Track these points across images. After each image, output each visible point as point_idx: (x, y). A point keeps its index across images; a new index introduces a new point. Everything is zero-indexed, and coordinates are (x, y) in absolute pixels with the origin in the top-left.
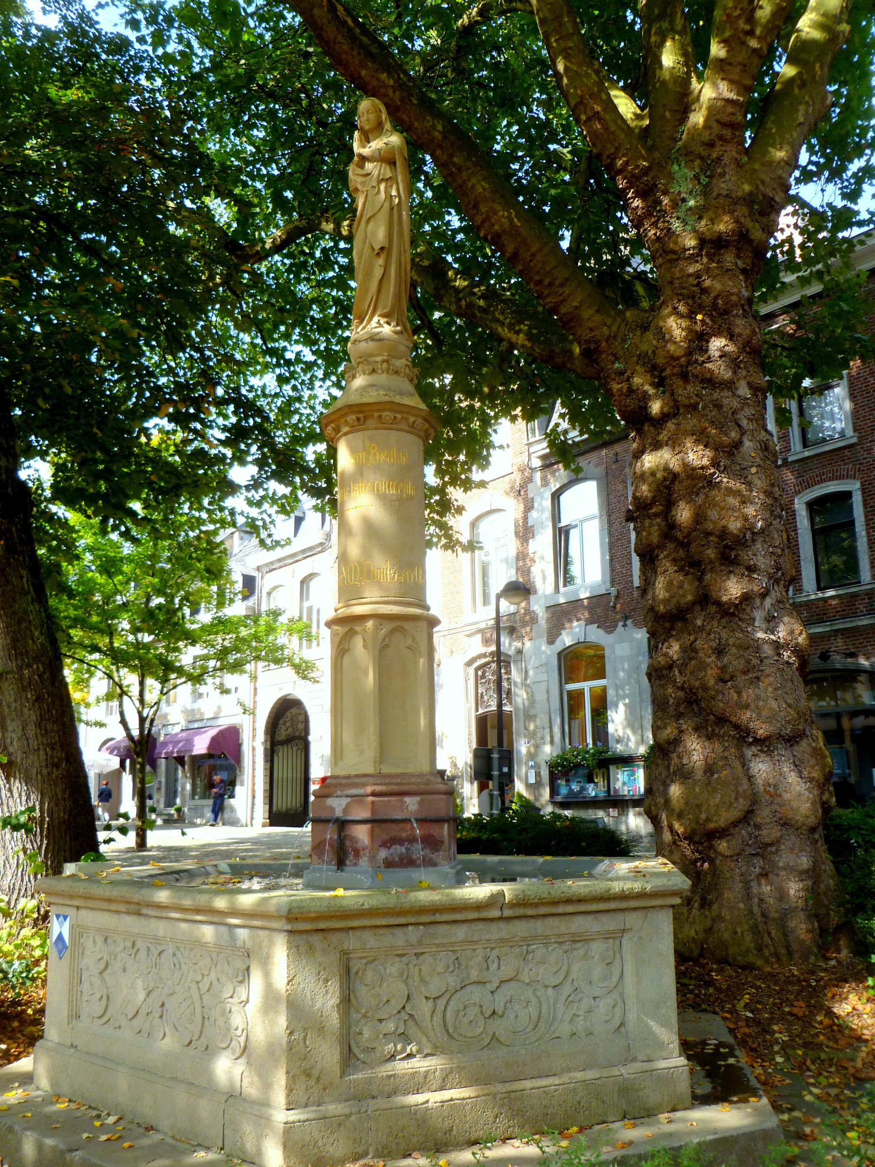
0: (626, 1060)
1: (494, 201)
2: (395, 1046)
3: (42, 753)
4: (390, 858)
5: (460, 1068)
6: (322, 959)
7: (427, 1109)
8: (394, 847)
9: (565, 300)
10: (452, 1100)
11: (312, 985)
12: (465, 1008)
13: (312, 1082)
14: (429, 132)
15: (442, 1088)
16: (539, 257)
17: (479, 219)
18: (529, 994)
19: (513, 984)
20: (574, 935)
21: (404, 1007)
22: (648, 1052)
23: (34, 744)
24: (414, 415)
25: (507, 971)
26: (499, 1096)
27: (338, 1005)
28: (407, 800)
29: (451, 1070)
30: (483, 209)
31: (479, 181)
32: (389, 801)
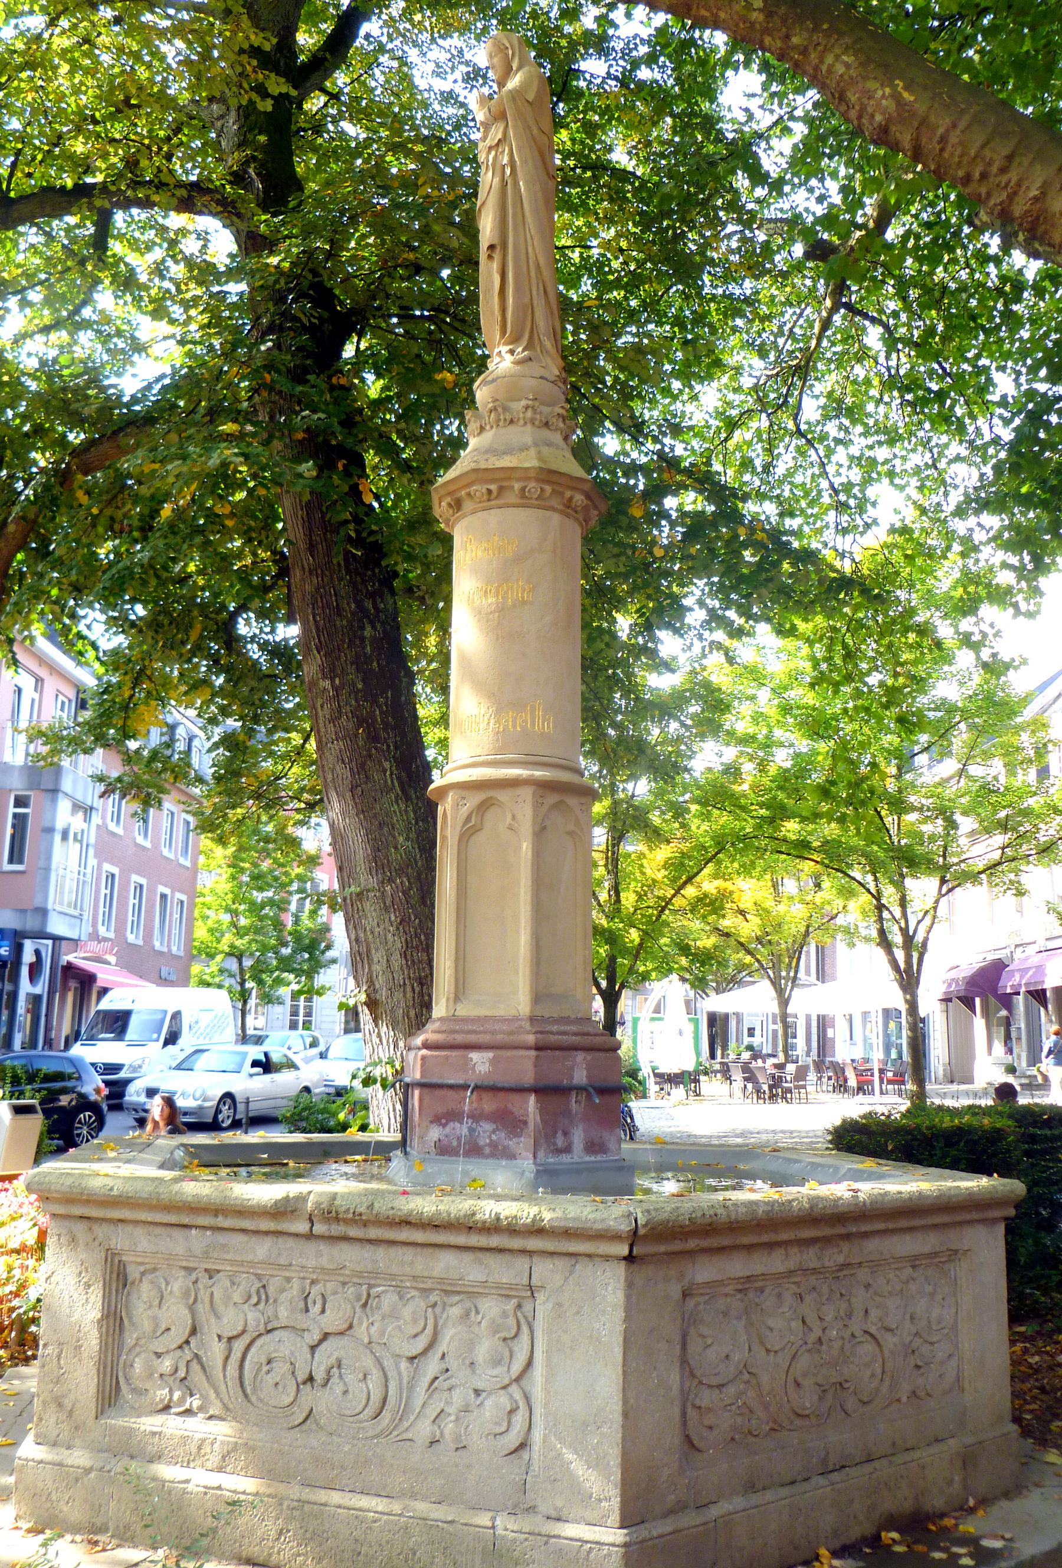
0: (516, 1506)
1: (865, 78)
2: (171, 1392)
3: (409, 989)
4: (445, 1142)
5: (248, 1448)
6: (83, 1256)
7: (184, 1492)
8: (451, 1125)
9: (1015, 193)
10: (219, 1488)
11: (72, 1288)
12: (269, 1362)
13: (63, 1416)
14: (744, 19)
15: (220, 1469)
16: (953, 139)
17: (853, 114)
18: (369, 1362)
19: (344, 1341)
20: (441, 1280)
21: (187, 1342)
22: (560, 1503)
23: (399, 977)
24: (518, 480)
25: (332, 1320)
26: (286, 1504)
27: (99, 1321)
28: (475, 1056)
29: (235, 1447)
30: (853, 97)
31: (837, 57)
32: (447, 1057)
